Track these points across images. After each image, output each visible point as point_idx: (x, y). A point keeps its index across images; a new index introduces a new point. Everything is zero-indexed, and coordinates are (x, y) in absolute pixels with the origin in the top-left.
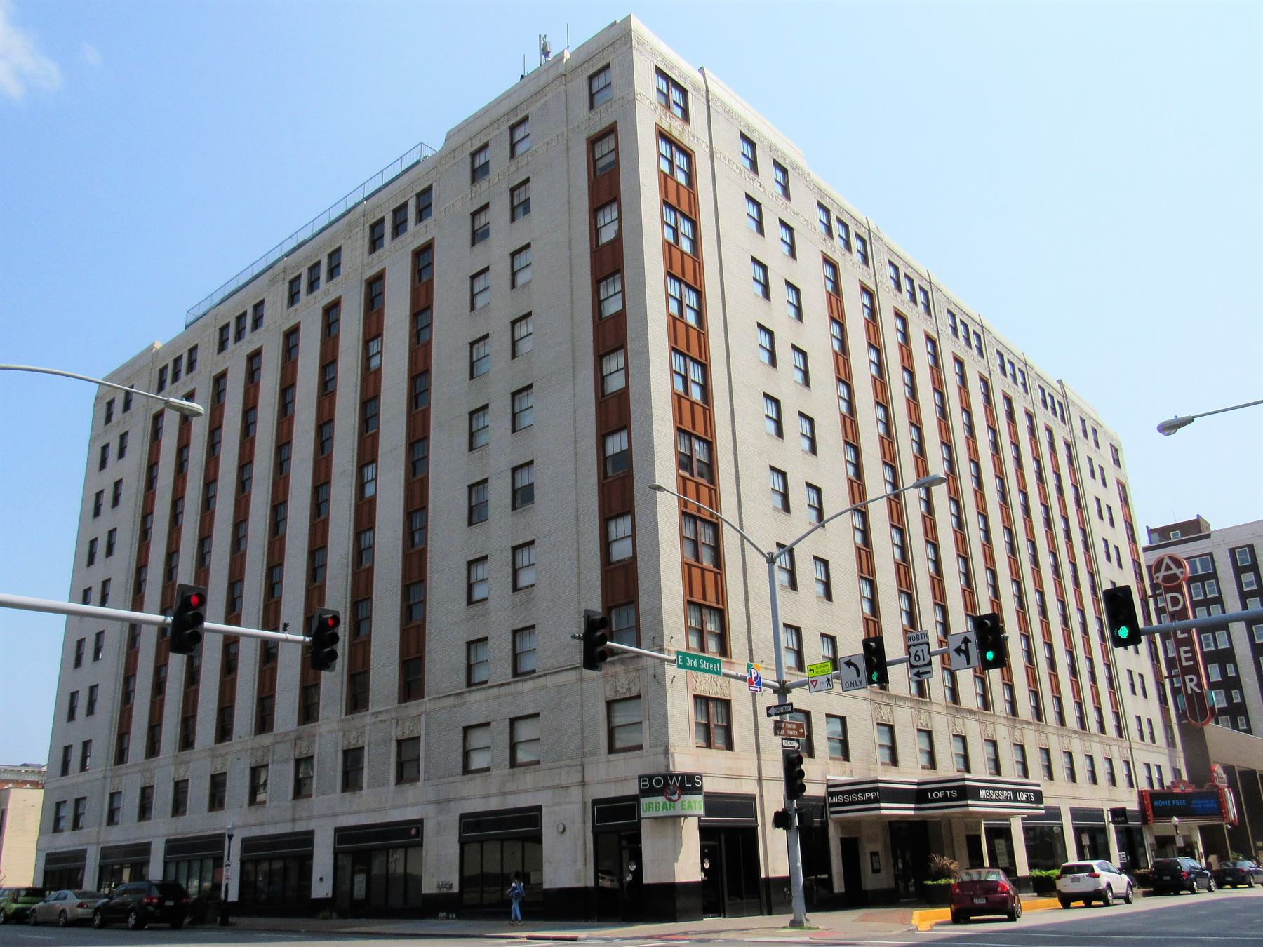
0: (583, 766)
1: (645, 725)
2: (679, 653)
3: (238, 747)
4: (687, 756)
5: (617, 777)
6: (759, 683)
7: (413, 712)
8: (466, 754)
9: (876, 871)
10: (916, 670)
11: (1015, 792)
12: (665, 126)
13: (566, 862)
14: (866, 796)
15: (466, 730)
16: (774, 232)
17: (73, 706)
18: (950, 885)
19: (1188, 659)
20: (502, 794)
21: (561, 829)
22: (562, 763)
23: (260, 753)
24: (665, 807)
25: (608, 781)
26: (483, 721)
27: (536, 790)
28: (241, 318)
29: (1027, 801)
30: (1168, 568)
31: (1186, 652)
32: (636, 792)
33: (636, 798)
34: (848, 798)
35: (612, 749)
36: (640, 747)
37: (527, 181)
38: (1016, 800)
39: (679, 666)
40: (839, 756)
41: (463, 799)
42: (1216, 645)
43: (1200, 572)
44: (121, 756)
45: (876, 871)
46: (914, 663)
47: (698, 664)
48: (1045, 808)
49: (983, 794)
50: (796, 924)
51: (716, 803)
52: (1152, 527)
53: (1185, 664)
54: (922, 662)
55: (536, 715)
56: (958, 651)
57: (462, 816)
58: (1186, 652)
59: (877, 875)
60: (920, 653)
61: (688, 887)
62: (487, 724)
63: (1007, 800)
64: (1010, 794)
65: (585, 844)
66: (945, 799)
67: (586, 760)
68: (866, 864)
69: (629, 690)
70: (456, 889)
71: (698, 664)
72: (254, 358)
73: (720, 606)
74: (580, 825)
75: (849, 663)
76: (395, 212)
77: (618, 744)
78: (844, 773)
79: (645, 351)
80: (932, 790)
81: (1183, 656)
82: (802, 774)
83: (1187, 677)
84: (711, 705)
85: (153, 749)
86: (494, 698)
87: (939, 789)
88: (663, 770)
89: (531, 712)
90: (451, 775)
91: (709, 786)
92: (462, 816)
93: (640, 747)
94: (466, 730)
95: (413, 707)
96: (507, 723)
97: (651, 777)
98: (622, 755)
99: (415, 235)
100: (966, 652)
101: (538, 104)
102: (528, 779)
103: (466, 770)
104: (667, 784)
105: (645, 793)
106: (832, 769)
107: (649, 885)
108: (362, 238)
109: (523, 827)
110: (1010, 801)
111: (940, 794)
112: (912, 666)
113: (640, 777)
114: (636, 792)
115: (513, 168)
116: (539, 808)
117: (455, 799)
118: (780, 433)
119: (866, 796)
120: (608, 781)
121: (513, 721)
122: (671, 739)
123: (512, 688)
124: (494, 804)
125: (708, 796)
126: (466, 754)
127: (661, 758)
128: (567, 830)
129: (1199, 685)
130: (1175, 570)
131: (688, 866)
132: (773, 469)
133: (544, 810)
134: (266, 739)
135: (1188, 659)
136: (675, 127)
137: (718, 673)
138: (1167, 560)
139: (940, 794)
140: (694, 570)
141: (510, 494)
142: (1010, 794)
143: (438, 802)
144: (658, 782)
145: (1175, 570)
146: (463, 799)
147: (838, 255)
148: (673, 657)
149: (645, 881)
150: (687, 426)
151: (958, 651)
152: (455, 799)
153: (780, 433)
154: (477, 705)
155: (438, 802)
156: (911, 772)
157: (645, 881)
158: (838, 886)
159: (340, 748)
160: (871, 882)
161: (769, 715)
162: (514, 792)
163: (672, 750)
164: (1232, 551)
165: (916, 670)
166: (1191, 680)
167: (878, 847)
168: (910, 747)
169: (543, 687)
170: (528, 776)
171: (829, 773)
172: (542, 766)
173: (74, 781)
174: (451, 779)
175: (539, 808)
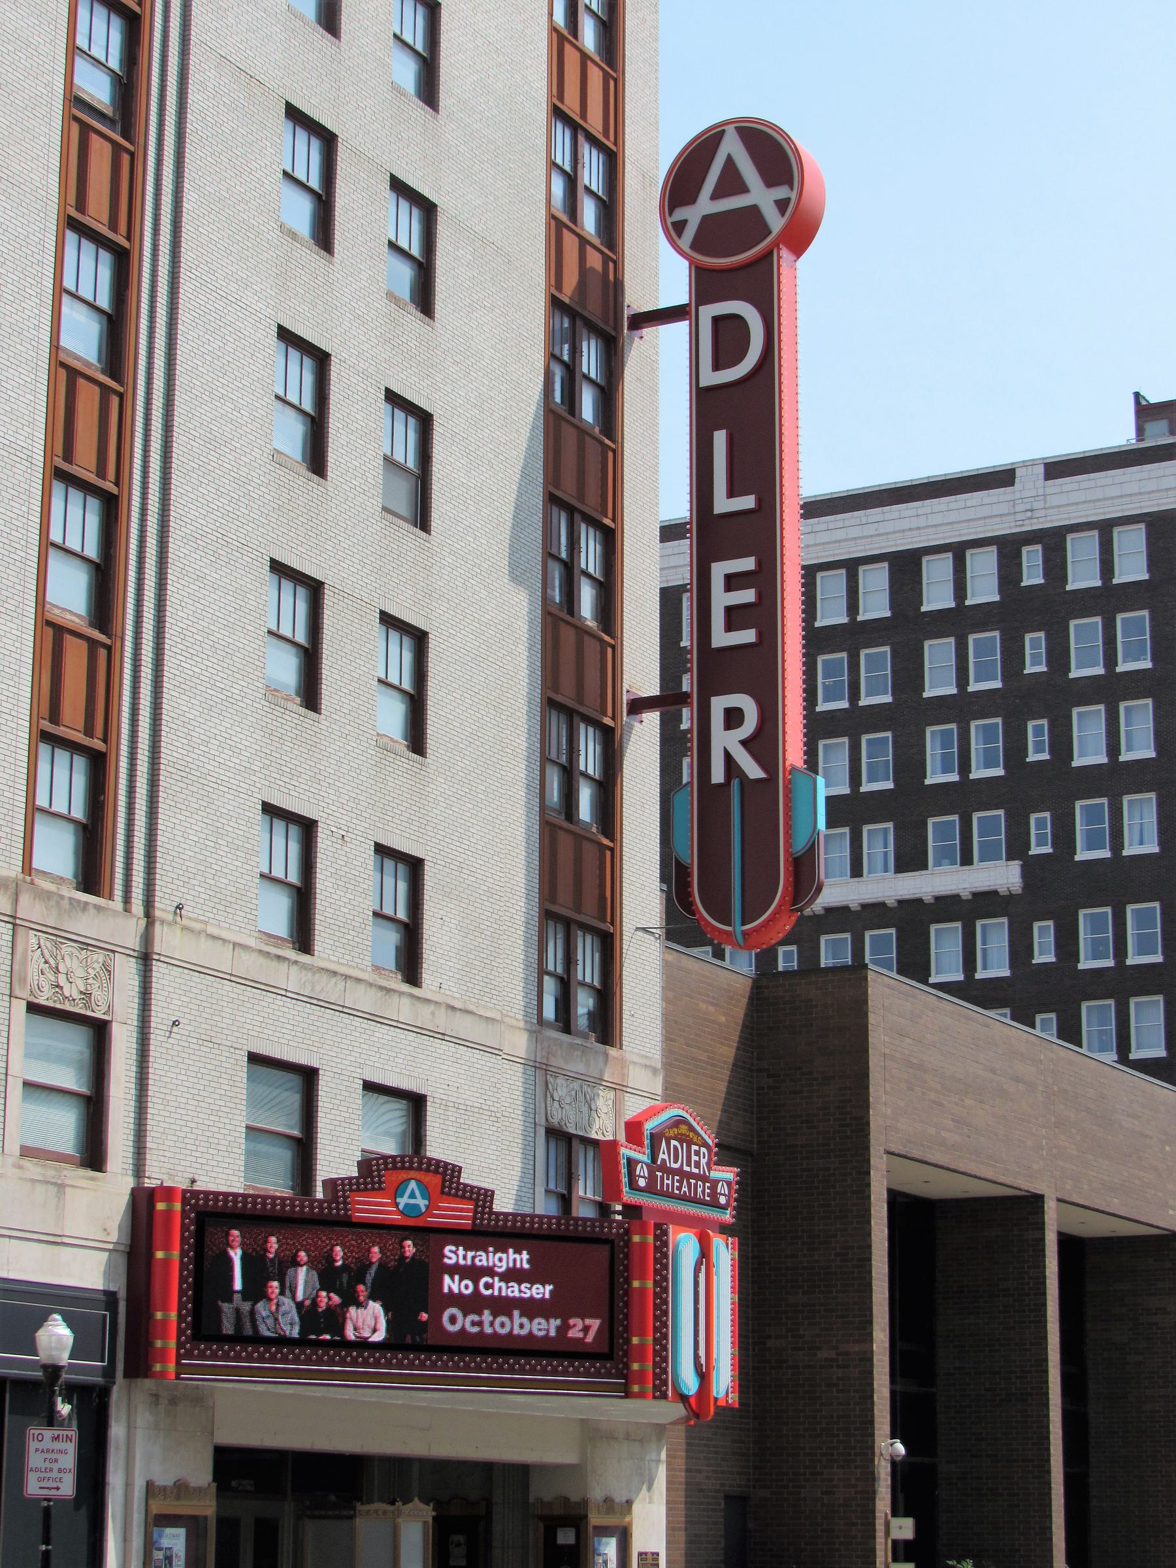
17: (207, 1193)
19: (735, 617)
30: (731, 183)
31: (733, 582)
42: (1113, 748)
53: (721, 638)
58: (733, 582)
73: (97, 744)
79: (653, 426)
81: (721, 599)
83: (719, 704)
118: (323, 234)
129: (764, 743)
130: (760, 195)
132: (286, 335)
135: (735, 617)
138: (732, 146)
140: (561, 835)
145: (760, 195)
150: (568, 492)
153: (323, 234)
166: (733, 718)
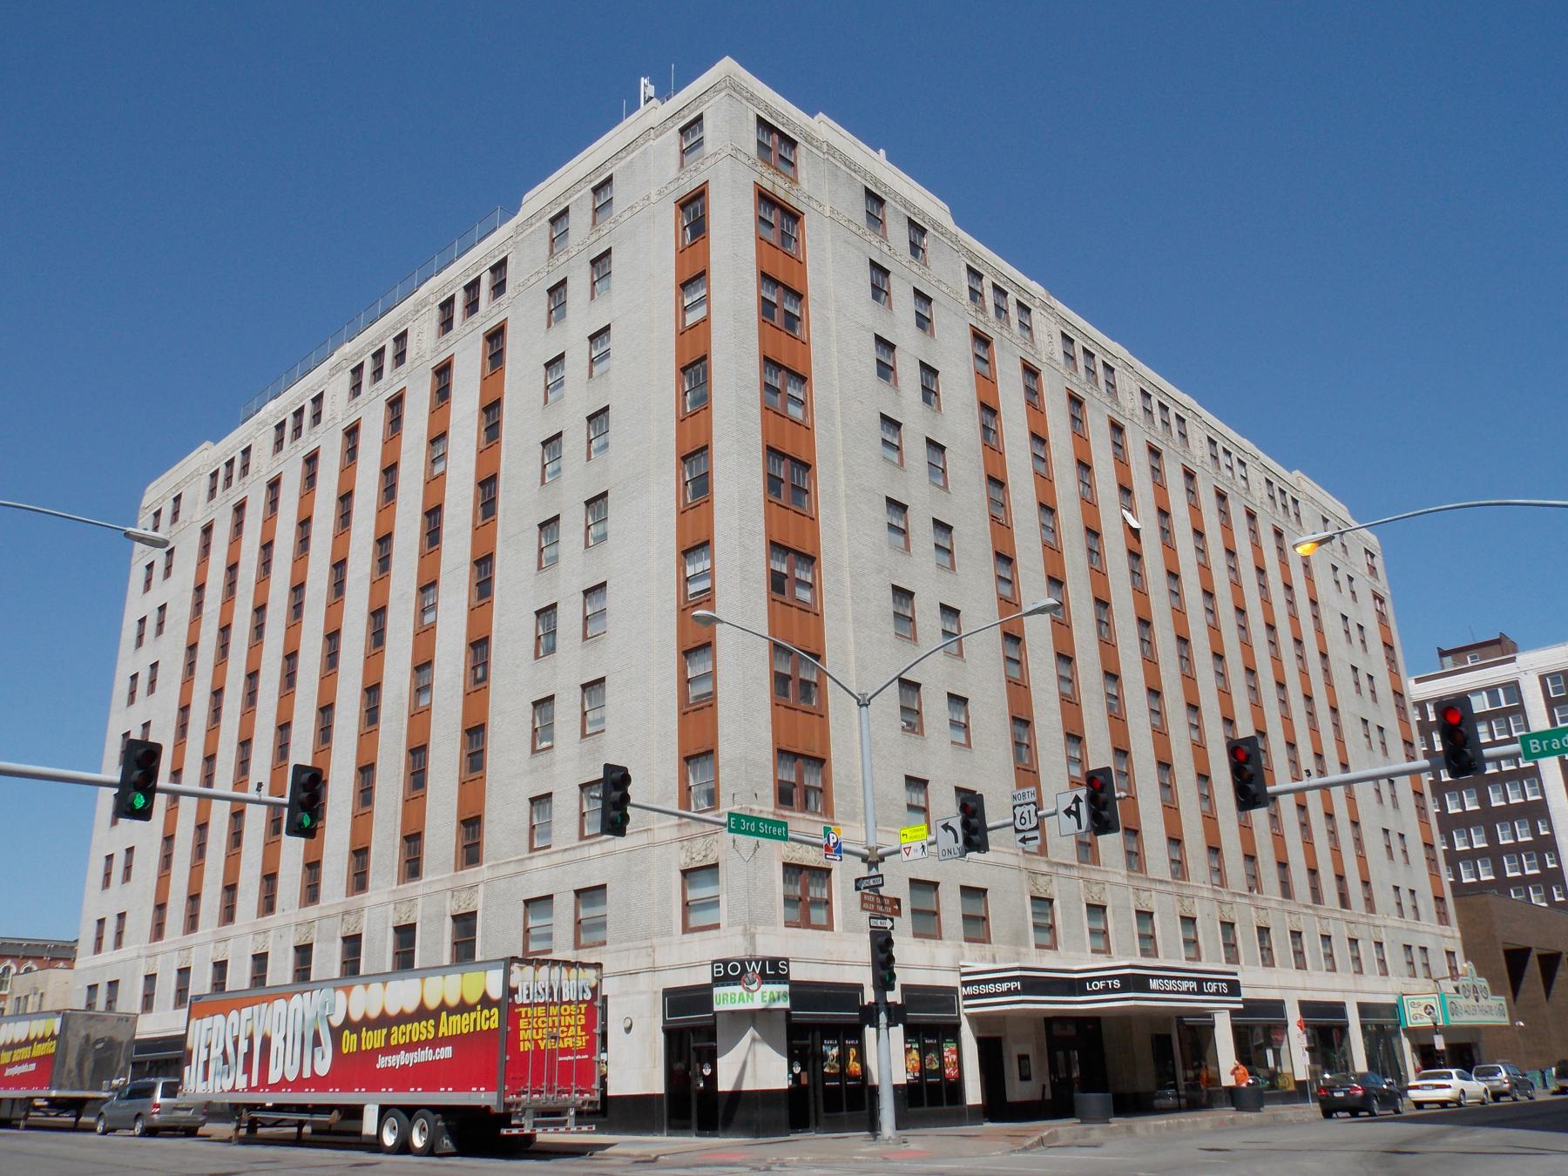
2: (731, 814)
3: (282, 922)
6: (839, 851)
7: (470, 881)
9: (1025, 1077)
10: (1021, 836)
11: (1200, 981)
12: (767, 185)
14: (1005, 987)
16: (904, 305)
18: (593, 1082)
22: (630, 944)
23: (304, 929)
24: (741, 999)
28: (299, 413)
29: (1217, 993)
32: (709, 980)
33: (707, 989)
34: (985, 989)
35: (686, 929)
36: (717, 926)
37: (608, 252)
38: (1200, 992)
39: (730, 830)
43: (1504, 705)
44: (158, 931)
45: (1025, 1077)
46: (1020, 827)
47: (757, 827)
48: (1245, 1001)
49: (1154, 984)
52: (1445, 649)
54: (1028, 826)
56: (1068, 812)
59: (1026, 1083)
60: (1026, 815)
63: (1188, 992)
64: (1193, 985)
66: (1106, 990)
68: (1011, 1069)
71: (757, 827)
72: (311, 460)
75: (946, 827)
76: (468, 288)
77: (692, 924)
78: (983, 959)
80: (1091, 980)
85: (192, 923)
86: (557, 865)
87: (1099, 979)
91: (798, 973)
95: (471, 875)
97: (725, 962)
98: (697, 935)
99: (490, 312)
100: (1077, 814)
101: (623, 163)
104: (744, 971)
105: (719, 981)
106: (967, 953)
107: (724, 1093)
108: (764, 228)
110: (1193, 993)
111: (1101, 985)
112: (1017, 831)
113: (714, 962)
114: (709, 980)
119: (1005, 987)
123: (578, 854)
125: (796, 985)
134: (312, 912)
136: (778, 186)
137: (785, 838)
139: (1101, 985)
141: (581, 621)
142: (1193, 985)
144: (734, 968)
147: (991, 328)
148: (724, 820)
151: (1068, 812)
154: (541, 876)
156: (1125, 956)
158: (973, 1094)
159: (391, 925)
160: (1017, 1091)
161: (857, 889)
164: (1542, 678)
165: (1021, 836)
167: (1028, 1049)
168: (1121, 926)
169: (611, 853)
171: (963, 957)
173: (107, 960)
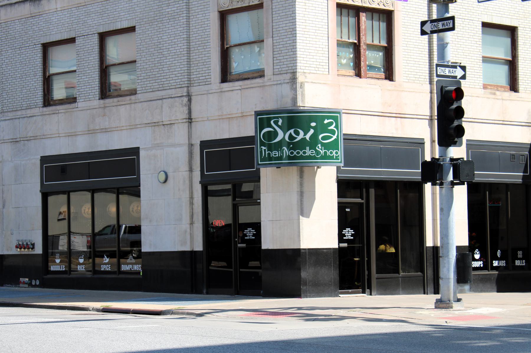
0: (189, 96)
1: (268, 42)
4: (322, 81)
5: (229, 114)
8: (47, 81)
13: (170, 217)
15: (46, 47)
20: (91, 132)
21: (162, 177)
25: (221, 118)
26: (66, 36)
27: (133, 127)
36: (260, 74)
40: (352, 72)
41: (44, 137)
50: (441, 304)
51: (360, 148)
55: (132, 29)
57: (44, 160)
61: (318, 255)
62: (72, 40)
65: (192, 198)
67: (194, 90)
69: (3, 137)
70: (39, 250)
74: (186, 174)
82: (460, 112)
84: (363, 17)
88: (289, 106)
89: (125, 25)
90: (29, 108)
91: (352, 126)
92: (44, 160)
93: (260, 74)
94: (46, 47)
96: (96, 40)
102: (120, 112)
103: (48, 101)
109: (117, 172)
115: (137, 58)
116: (136, 151)
117: (35, 138)
120: (221, 118)
121: (103, 37)
122: (302, 66)
124: (81, 145)
126: (47, 81)
127: (286, 89)
128: (170, 175)
131: (320, 229)
133: (142, 153)
143: (15, 141)
146: (44, 137)
149: (264, 246)
152: (35, 138)
155: (15, 141)
157: (264, 246)
162: (105, 131)
163: (300, 78)
170: (122, 109)
172: (140, 97)
174: (29, 112)
175: (136, 151)
